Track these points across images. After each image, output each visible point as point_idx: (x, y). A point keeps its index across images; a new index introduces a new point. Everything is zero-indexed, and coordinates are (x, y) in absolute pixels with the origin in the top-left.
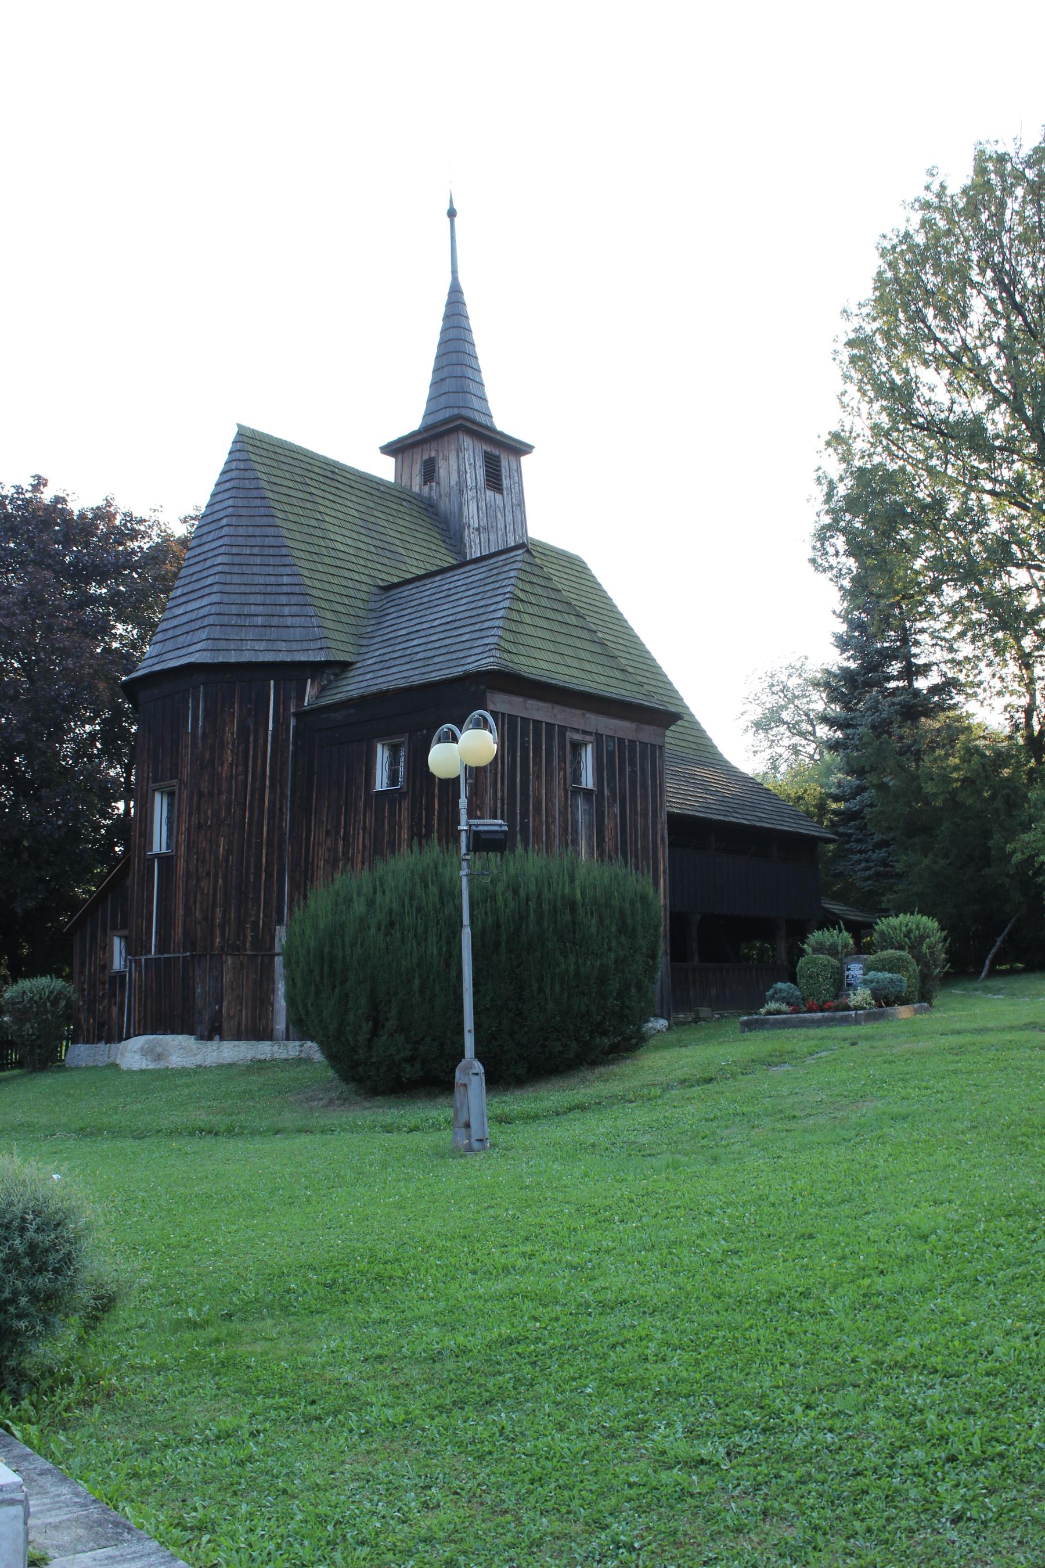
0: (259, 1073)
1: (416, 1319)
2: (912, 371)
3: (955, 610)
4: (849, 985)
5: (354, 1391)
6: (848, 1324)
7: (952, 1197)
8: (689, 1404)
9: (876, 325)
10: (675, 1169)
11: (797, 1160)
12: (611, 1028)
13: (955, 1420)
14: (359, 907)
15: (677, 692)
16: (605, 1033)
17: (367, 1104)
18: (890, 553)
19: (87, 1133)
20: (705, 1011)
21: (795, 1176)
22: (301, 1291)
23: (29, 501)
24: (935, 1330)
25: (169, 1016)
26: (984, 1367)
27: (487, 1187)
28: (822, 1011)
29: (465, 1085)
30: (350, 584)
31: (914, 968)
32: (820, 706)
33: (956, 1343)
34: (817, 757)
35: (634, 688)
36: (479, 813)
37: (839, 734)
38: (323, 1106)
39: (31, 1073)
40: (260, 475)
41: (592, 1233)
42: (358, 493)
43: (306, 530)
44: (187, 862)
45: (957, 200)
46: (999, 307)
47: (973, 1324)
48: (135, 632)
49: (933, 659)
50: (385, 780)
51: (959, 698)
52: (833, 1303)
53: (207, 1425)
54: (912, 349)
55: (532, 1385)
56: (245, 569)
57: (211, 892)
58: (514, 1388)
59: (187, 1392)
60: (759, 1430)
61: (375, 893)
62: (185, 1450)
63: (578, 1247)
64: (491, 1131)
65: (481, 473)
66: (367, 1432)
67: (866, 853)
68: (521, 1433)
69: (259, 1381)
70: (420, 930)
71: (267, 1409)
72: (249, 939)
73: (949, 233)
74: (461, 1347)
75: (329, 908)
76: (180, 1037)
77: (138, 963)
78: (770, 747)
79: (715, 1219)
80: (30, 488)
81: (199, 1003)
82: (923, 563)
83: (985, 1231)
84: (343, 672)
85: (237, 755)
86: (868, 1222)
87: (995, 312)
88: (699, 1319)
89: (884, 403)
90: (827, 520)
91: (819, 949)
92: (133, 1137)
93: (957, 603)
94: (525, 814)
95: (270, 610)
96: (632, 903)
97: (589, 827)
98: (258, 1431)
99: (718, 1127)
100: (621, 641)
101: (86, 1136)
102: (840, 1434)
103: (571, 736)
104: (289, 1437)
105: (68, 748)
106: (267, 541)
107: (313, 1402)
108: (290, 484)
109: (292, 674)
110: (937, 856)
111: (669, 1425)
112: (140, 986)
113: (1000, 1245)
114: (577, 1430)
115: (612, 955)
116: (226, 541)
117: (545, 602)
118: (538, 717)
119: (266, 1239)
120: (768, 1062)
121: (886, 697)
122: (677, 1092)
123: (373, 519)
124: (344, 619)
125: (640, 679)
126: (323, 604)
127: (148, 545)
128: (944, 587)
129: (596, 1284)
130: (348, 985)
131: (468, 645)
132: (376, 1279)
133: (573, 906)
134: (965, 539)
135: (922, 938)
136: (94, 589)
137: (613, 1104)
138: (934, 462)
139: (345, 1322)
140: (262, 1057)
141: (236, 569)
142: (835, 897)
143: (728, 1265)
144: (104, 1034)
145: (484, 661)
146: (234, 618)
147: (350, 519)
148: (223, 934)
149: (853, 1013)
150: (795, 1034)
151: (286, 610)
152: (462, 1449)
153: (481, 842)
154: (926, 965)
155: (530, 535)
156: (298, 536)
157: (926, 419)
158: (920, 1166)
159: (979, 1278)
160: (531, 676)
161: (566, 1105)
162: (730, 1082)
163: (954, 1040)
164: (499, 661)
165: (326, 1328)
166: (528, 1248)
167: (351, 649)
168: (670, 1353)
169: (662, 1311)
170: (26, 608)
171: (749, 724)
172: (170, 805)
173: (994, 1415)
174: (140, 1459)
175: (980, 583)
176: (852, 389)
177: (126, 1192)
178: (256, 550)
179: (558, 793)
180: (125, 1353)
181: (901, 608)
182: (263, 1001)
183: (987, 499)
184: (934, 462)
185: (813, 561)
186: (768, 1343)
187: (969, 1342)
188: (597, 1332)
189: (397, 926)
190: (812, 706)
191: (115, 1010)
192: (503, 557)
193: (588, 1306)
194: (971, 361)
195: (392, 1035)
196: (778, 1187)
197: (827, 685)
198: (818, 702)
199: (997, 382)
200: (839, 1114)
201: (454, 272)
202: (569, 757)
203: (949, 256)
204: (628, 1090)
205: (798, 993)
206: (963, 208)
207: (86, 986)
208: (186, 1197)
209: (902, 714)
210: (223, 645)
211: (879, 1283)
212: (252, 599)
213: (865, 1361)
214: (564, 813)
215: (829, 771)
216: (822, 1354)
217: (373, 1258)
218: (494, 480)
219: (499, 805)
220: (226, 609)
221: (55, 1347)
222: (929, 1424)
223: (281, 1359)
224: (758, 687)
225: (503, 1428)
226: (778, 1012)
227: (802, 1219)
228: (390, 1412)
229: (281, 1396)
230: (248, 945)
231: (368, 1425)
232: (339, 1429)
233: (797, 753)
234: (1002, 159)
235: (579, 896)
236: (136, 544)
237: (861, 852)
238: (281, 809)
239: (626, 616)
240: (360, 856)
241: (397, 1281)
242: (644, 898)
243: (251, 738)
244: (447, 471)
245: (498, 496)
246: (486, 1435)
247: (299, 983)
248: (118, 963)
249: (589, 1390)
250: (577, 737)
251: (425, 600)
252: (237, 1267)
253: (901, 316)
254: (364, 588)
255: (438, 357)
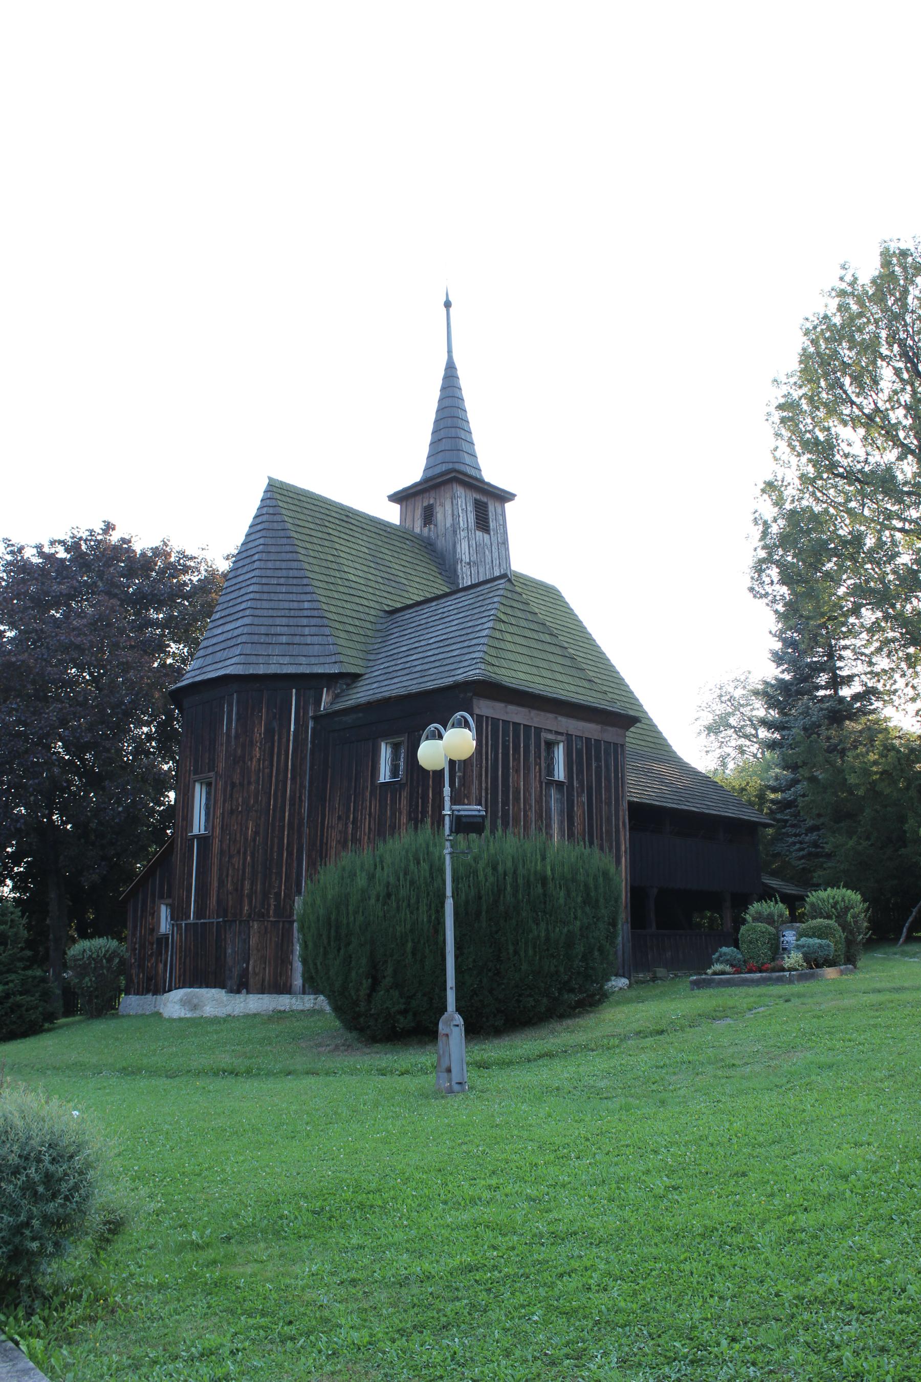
0: (278, 1022)
1: (390, 1246)
2: (833, 430)
3: (873, 629)
4: (784, 949)
5: (326, 1313)
6: (773, 1259)
7: (871, 1140)
8: (625, 1334)
9: (801, 392)
10: (627, 1111)
11: (734, 1104)
12: (577, 986)
13: (870, 1358)
14: (361, 881)
15: (637, 700)
16: (572, 990)
17: (367, 1050)
18: (817, 581)
19: (129, 1072)
20: (661, 972)
21: (732, 1119)
22: (292, 1217)
23: (99, 542)
24: (852, 1268)
25: (205, 971)
26: (897, 1305)
27: (463, 1125)
28: (760, 972)
29: (447, 1035)
30: (361, 609)
31: (840, 934)
32: (761, 713)
33: (872, 1280)
34: (759, 755)
35: (600, 696)
36: (466, 801)
37: (777, 736)
38: (329, 1052)
39: (89, 1019)
40: (286, 519)
41: (551, 1168)
42: (368, 533)
43: (324, 564)
44: (221, 841)
45: (868, 289)
46: (906, 376)
47: (888, 1262)
48: (186, 650)
49: (855, 671)
50: (388, 773)
51: (877, 704)
52: (760, 1238)
53: (193, 1342)
54: (832, 411)
55: (485, 1311)
56: (273, 596)
57: (241, 867)
58: (470, 1314)
59: (180, 1310)
60: (687, 1362)
61: (375, 868)
62: (171, 1367)
63: (536, 1181)
64: (472, 1076)
65: (472, 517)
66: (334, 1354)
67: (800, 836)
68: (471, 1358)
69: (244, 1301)
70: (413, 901)
71: (248, 1329)
72: (273, 907)
73: (861, 315)
74: (426, 1274)
75: (336, 881)
76: (213, 990)
77: (179, 927)
78: (720, 747)
79: (660, 1157)
80: (101, 532)
81: (230, 961)
82: (845, 590)
83: (900, 1172)
84: (354, 682)
85: (264, 751)
86: (795, 1162)
87: (902, 380)
88: (639, 1251)
89: (810, 456)
90: (763, 554)
91: (758, 918)
92: (167, 1077)
93: (873, 623)
94: (506, 803)
95: (292, 630)
96: (595, 878)
97: (561, 813)
98: (238, 1350)
99: (667, 1074)
100: (590, 657)
101: (128, 1075)
102: (762, 1368)
103: (544, 735)
104: (264, 1356)
105: (128, 747)
106: (291, 573)
107: (290, 1323)
108: (312, 526)
109: (311, 683)
110: (860, 838)
111: (605, 1354)
112: (181, 947)
113: (913, 1186)
114: (521, 1357)
115: (578, 923)
116: (256, 573)
117: (523, 623)
118: (517, 720)
119: (267, 1169)
120: (713, 1017)
121: (815, 703)
122: (633, 1042)
123: (381, 555)
124: (355, 638)
125: (605, 688)
126: (337, 625)
127: (197, 578)
128: (863, 610)
129: (551, 1216)
130: (351, 947)
131: (458, 659)
132: (358, 1207)
133: (544, 881)
134: (880, 569)
135: (847, 909)
136: (153, 614)
137: (577, 1052)
138: (853, 504)
139: (327, 1246)
140: (282, 1008)
141: (265, 596)
142: (774, 874)
143: (669, 1200)
144: (152, 987)
145: (471, 673)
146: (263, 637)
147: (361, 555)
148: (250, 904)
149: (787, 974)
150: (737, 992)
151: (307, 631)
152: (416, 1372)
153: (463, 826)
154: (851, 932)
155: (513, 568)
156: (317, 569)
157: (845, 469)
158: (843, 1111)
159: (894, 1217)
160: (510, 685)
161: (537, 1053)
162: (679, 1034)
163: (874, 998)
164: (484, 672)
165: (310, 1252)
166: (494, 1182)
167: (360, 663)
168: (612, 1284)
169: (607, 1242)
170: (95, 630)
171: (702, 728)
172: (208, 794)
173: (906, 1353)
174: (130, 1374)
175: (893, 606)
176: (783, 445)
177: (153, 1124)
178: (282, 581)
179: (534, 785)
180: (133, 1271)
181: (827, 628)
182: (284, 961)
183: (898, 536)
184: (853, 504)
185: (751, 589)
186: (699, 1276)
187: (884, 1279)
188: (547, 1262)
189: (393, 897)
190: (755, 713)
191: (161, 966)
192: (489, 586)
193: (542, 1237)
194: (882, 420)
195: (388, 991)
196: (717, 1128)
197: (765, 694)
198: (760, 710)
199: (905, 439)
200: (773, 1063)
201: (450, 351)
202: (543, 754)
203: (862, 333)
204: (591, 1040)
205: (740, 956)
206: (873, 294)
207: (137, 946)
208: (204, 1129)
209: (829, 718)
210: (253, 659)
211: (804, 1220)
212: (278, 621)
213: (788, 1296)
214: (539, 801)
215: (768, 768)
216: (748, 1288)
217: (357, 1189)
218: (482, 523)
219: (483, 794)
220: (256, 629)
221: (69, 1265)
222: (845, 1361)
223: (268, 1280)
224: (710, 697)
225: (455, 1353)
226: (723, 973)
227: (737, 1158)
228: (355, 1334)
229: (263, 1316)
230: (271, 912)
231: (336, 1346)
232: (309, 1349)
233: (742, 752)
234: (904, 254)
235: (549, 873)
236: (188, 577)
237: (796, 835)
238: (300, 797)
239: (594, 636)
240: (366, 838)
241: (377, 1210)
242: (605, 874)
243: (276, 738)
244: (444, 516)
245: (486, 536)
246: (440, 1358)
247: (310, 945)
248: (164, 927)
249: (535, 1318)
250: (550, 737)
251: (423, 621)
252: (240, 1194)
253: (823, 383)
254: (372, 612)
255: (436, 421)
